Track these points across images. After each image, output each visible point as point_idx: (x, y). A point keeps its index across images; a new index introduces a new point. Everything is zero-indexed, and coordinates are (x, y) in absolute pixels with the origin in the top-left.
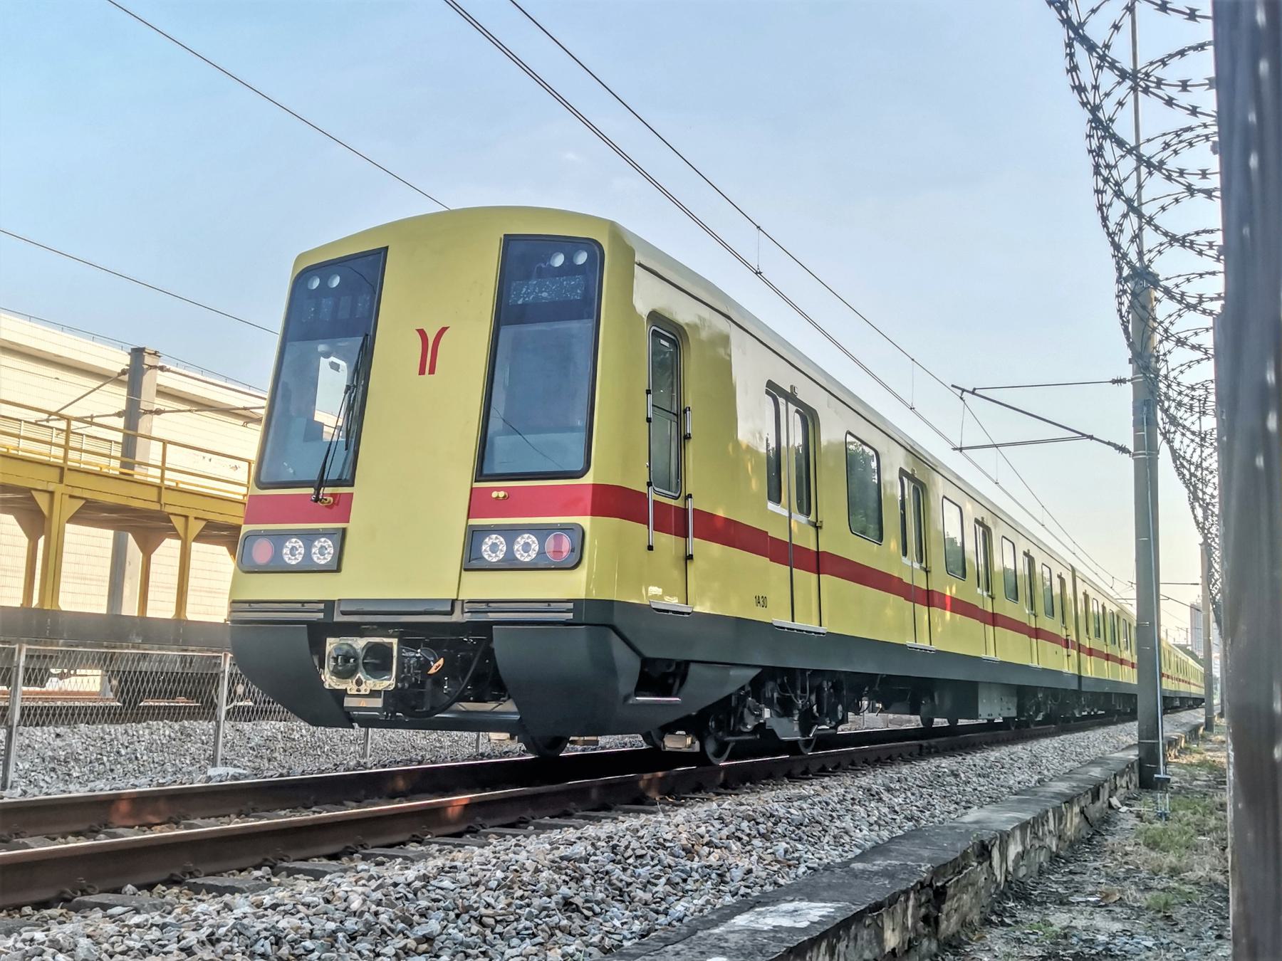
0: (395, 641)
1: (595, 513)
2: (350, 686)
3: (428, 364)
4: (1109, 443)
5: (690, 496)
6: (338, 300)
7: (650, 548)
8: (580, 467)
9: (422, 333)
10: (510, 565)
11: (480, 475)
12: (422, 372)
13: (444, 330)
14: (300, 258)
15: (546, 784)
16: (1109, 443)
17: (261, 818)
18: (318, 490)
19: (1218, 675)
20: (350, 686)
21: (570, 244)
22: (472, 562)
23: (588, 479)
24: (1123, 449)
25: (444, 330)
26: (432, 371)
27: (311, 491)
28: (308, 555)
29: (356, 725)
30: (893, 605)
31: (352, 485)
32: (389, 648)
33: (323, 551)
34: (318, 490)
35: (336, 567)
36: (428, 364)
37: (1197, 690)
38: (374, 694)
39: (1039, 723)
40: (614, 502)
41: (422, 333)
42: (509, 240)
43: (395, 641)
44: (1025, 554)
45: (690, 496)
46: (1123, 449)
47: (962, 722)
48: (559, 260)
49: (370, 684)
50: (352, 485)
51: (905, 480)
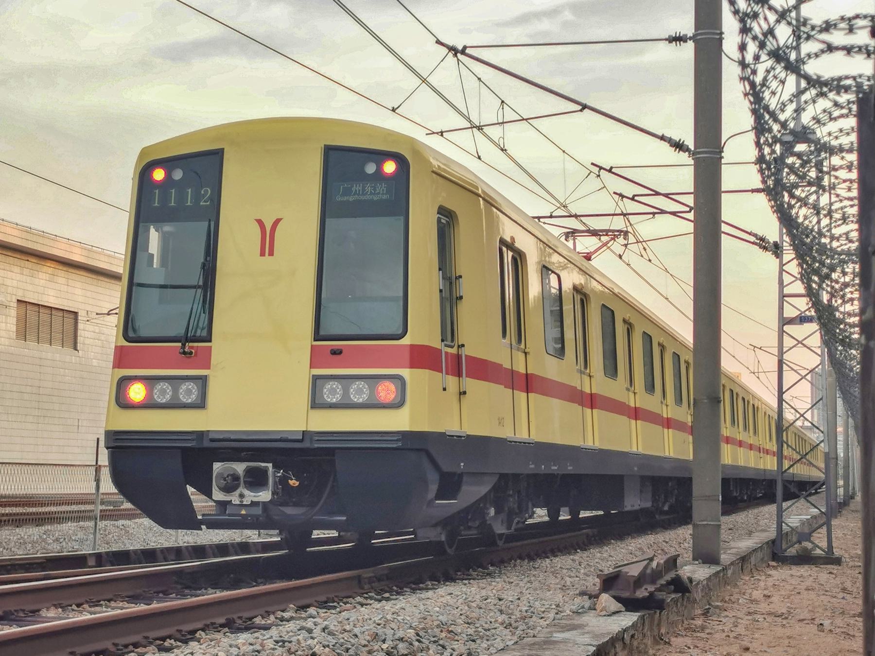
0: (270, 465)
1: (413, 365)
2: (235, 499)
3: (267, 246)
4: (662, 138)
5: (463, 346)
6: (181, 187)
7: (444, 389)
8: (400, 332)
9: (260, 222)
10: (346, 405)
11: (317, 337)
12: (262, 254)
13: (278, 221)
14: (144, 152)
15: (297, 572)
16: (662, 138)
17: (184, 596)
18: (184, 345)
19: (842, 455)
20: (235, 499)
21: (382, 156)
22: (316, 404)
23: (406, 341)
24: (679, 146)
25: (278, 221)
26: (271, 254)
27: (180, 344)
28: (175, 391)
29: (203, 527)
30: (556, 407)
31: (210, 341)
32: (265, 471)
33: (188, 393)
34: (184, 345)
35: (200, 404)
36: (267, 246)
37: (817, 474)
38: (254, 504)
39: (666, 513)
40: (422, 357)
41: (260, 222)
42: (329, 150)
43: (270, 465)
44: (625, 321)
45: (463, 346)
46: (679, 146)
47: (584, 514)
48: (371, 168)
49: (250, 496)
50: (210, 341)
51: (504, 249)
